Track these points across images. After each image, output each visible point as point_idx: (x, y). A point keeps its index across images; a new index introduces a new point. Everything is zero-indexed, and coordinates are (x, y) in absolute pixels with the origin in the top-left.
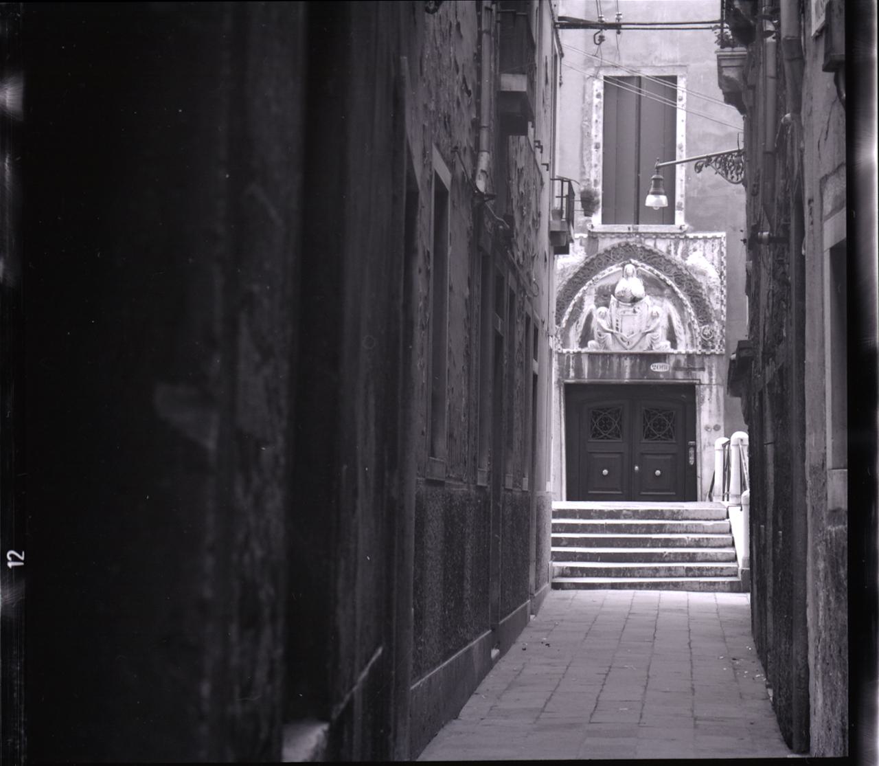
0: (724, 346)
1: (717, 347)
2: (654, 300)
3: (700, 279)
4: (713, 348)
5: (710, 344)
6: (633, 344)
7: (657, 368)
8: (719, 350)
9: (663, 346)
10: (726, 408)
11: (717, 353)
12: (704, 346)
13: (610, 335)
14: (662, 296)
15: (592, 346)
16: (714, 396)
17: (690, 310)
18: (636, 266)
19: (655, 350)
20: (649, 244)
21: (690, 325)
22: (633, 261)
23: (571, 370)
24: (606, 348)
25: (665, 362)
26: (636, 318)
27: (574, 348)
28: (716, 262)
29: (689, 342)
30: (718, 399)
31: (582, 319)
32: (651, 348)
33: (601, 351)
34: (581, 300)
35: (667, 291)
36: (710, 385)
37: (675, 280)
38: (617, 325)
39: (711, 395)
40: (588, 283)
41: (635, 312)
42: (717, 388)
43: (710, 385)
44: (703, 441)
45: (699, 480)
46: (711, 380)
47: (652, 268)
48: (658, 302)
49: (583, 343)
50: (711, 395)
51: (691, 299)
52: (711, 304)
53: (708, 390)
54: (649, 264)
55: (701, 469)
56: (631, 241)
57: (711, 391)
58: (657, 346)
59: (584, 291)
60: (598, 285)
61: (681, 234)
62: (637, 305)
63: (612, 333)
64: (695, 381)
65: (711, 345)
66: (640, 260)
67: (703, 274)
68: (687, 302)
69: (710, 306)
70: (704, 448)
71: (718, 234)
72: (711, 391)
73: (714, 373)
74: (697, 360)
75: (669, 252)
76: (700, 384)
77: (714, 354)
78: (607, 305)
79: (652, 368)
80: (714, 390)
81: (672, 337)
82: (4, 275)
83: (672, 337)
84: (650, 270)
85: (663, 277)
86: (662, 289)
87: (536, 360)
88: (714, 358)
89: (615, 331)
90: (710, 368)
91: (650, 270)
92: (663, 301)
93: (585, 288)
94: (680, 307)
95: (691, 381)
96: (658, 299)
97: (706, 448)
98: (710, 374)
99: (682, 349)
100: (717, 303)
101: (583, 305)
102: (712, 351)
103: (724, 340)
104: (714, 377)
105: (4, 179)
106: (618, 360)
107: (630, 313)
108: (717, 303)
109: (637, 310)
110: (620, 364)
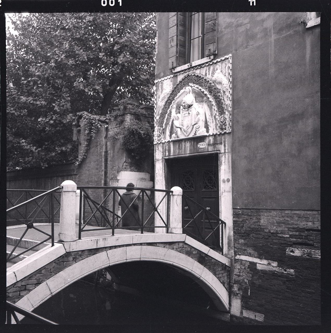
0: (231, 127)
1: (227, 128)
2: (200, 105)
3: (219, 87)
4: (225, 129)
5: (224, 127)
6: (189, 133)
7: (202, 145)
8: (228, 130)
9: (202, 132)
10: (232, 168)
11: (227, 132)
12: (222, 129)
13: (179, 129)
14: (202, 102)
15: (174, 137)
16: (226, 160)
17: (215, 108)
18: (191, 87)
19: (198, 135)
20: (198, 72)
21: (215, 117)
22: (190, 84)
23: (167, 151)
24: (178, 137)
25: (204, 142)
26: (190, 117)
27: (168, 139)
28: (227, 74)
29: (215, 128)
30: (229, 162)
31: (170, 123)
32: (195, 134)
33: (177, 139)
34: (171, 112)
35: (205, 98)
36: (225, 152)
37: (209, 90)
38: (182, 123)
39: (225, 159)
40: (173, 102)
41: (189, 114)
42: (228, 154)
43: (225, 152)
44: (221, 189)
45: (220, 213)
46: (225, 150)
47: (198, 86)
48: (201, 106)
49: (170, 136)
50: (225, 159)
51: (216, 100)
52: (225, 101)
53: (224, 156)
54: (197, 84)
55: (221, 205)
56: (191, 73)
57: (225, 157)
58: (199, 132)
59: (172, 106)
60: (177, 102)
61: (210, 62)
62: (190, 109)
63: (180, 128)
64: (218, 152)
65: (224, 128)
66: (194, 83)
67: (220, 83)
68: (214, 103)
69: (224, 103)
70: (222, 194)
71: (227, 57)
72: (225, 157)
73: (226, 145)
74: (218, 138)
75: (206, 74)
76: (220, 153)
77: (225, 133)
78: (179, 113)
79: (198, 146)
80: (227, 156)
81: (207, 127)
82: (129, 171)
83: (207, 127)
84: (197, 88)
85: (203, 90)
86: (203, 97)
87: (118, 182)
88: (226, 136)
89: (181, 127)
90: (225, 142)
91: (197, 88)
92: (203, 105)
93: (171, 105)
94: (210, 107)
95: (216, 152)
96: (201, 104)
97: (223, 193)
98: (225, 146)
99: (211, 133)
100: (227, 100)
101: (171, 114)
102: (225, 131)
103: (231, 124)
104: (226, 148)
105: (220, 246)
106: (184, 144)
107: (187, 115)
108: (227, 100)
109: (190, 112)
110: (185, 145)
